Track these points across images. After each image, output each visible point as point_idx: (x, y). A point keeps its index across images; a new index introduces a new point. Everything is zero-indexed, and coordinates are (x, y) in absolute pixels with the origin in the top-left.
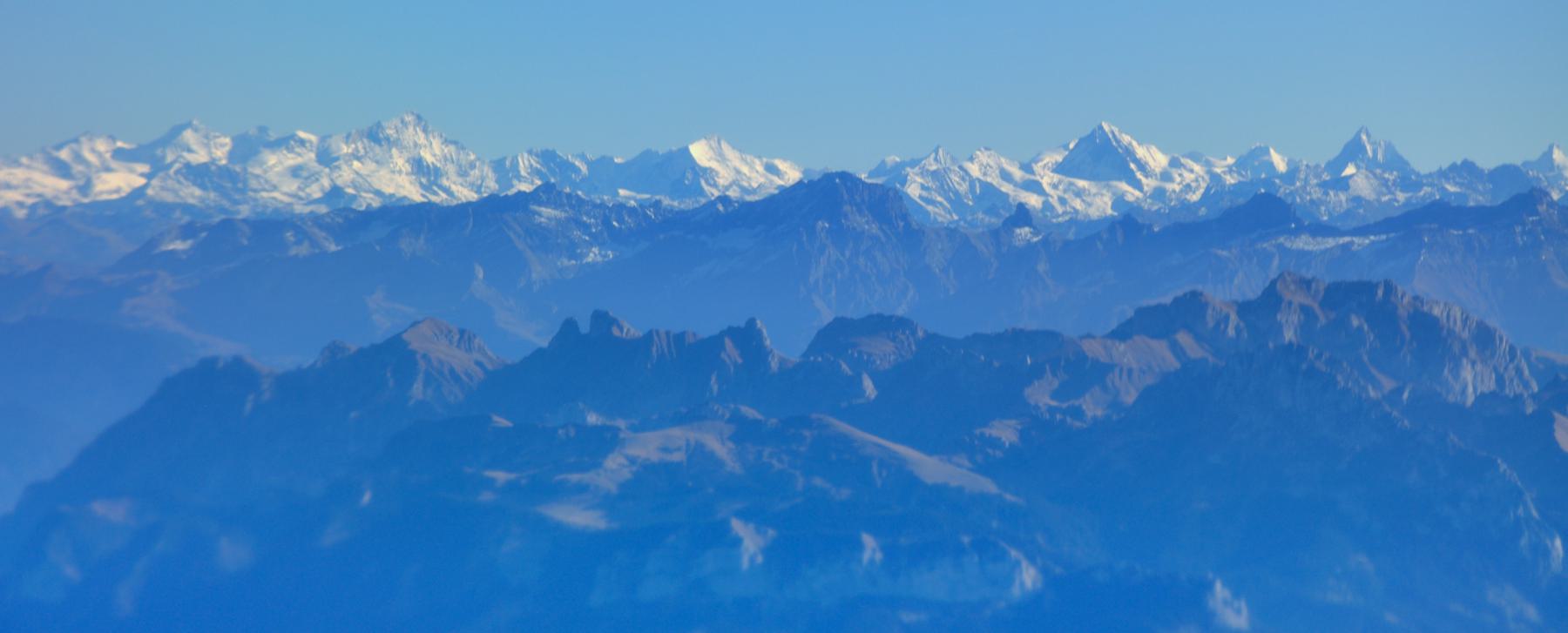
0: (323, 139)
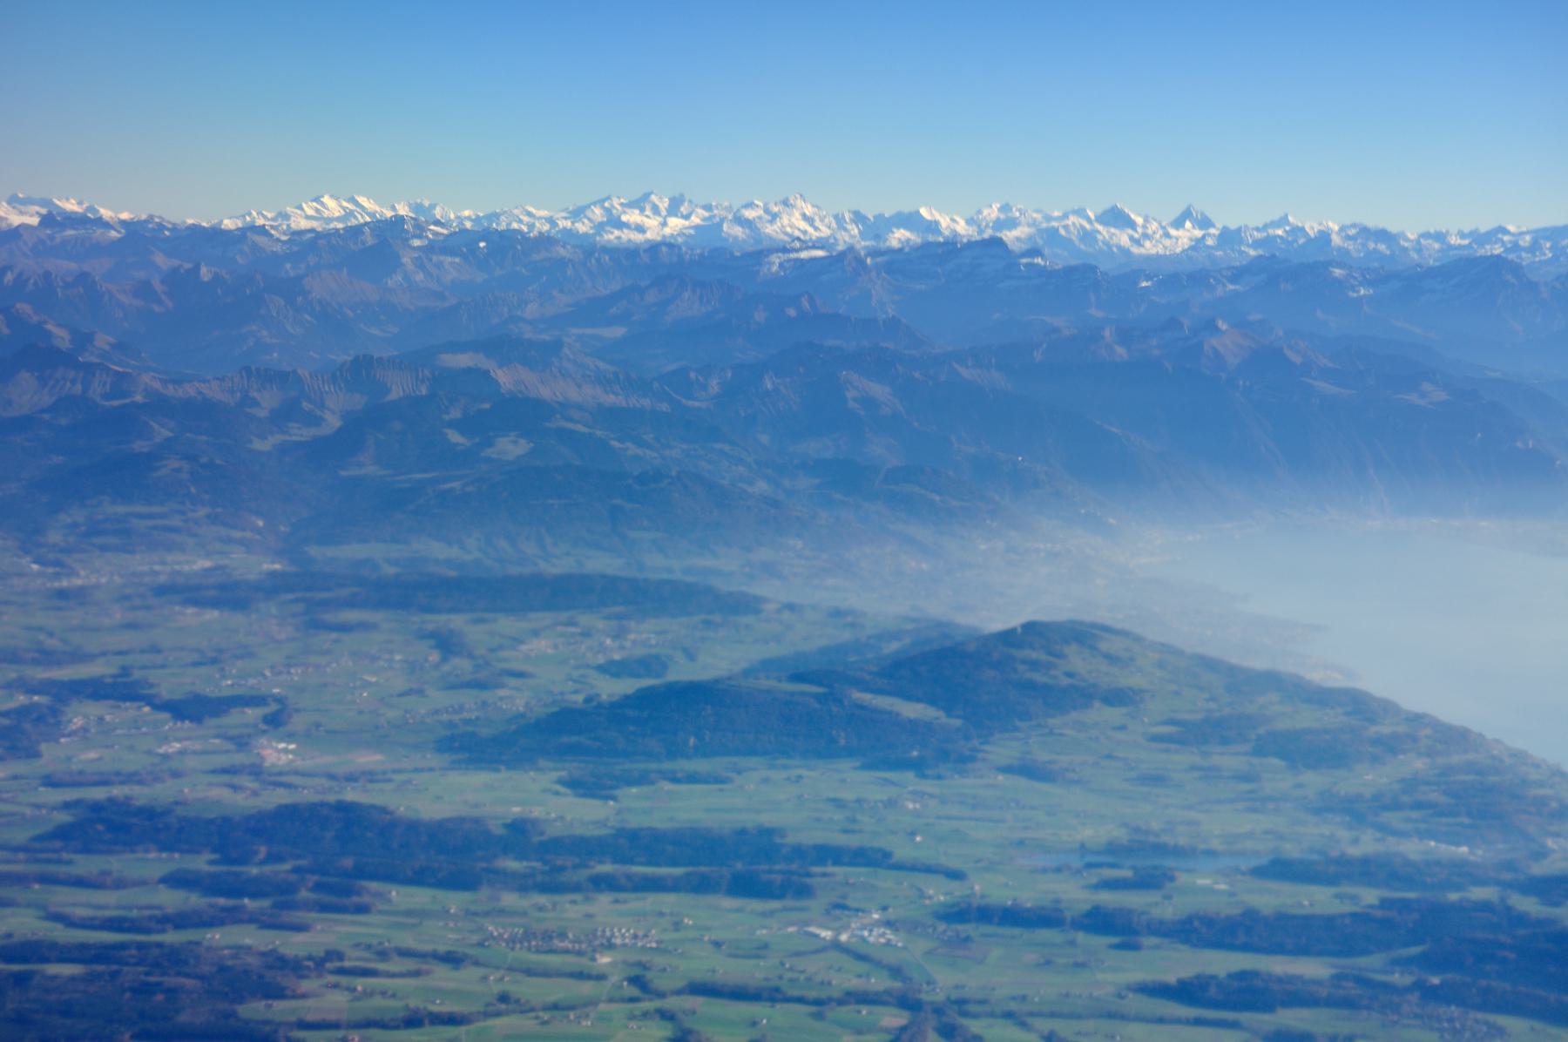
0: (765, 205)
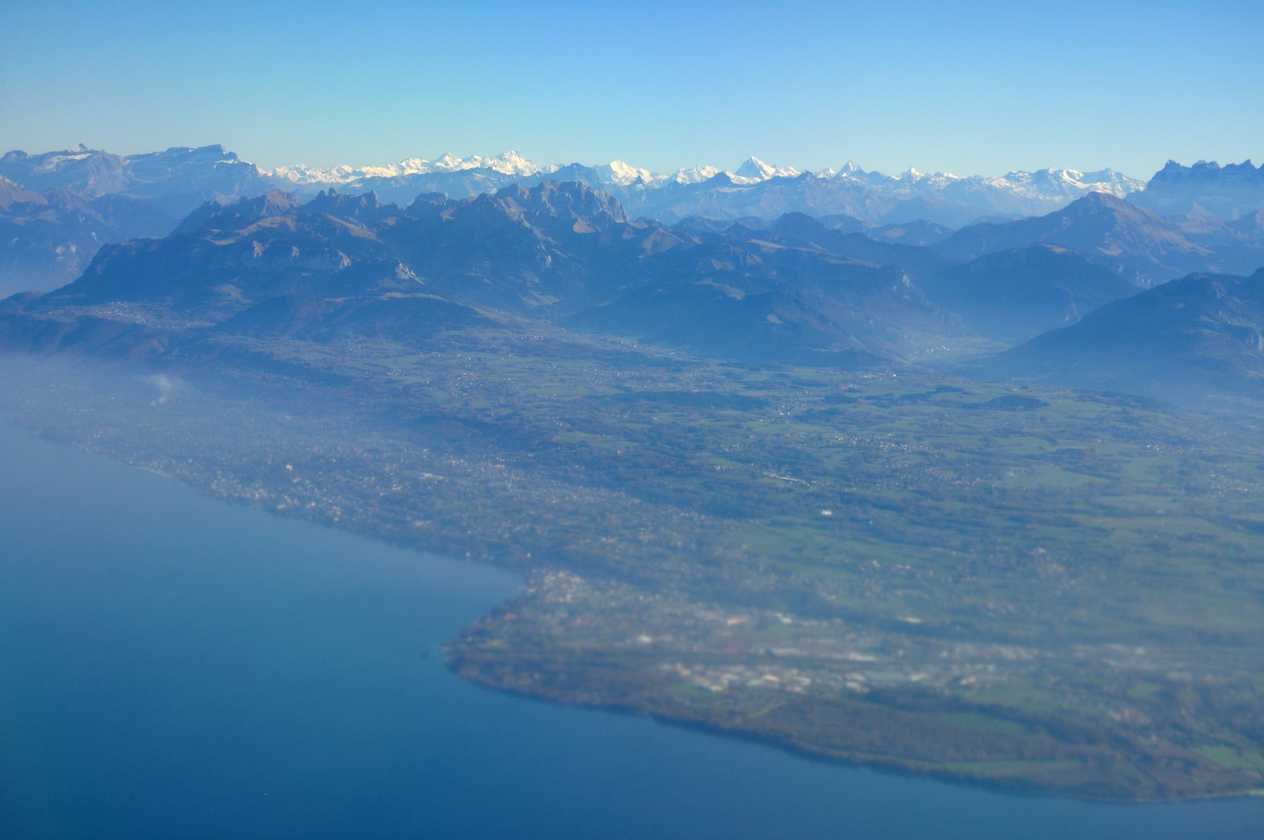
0: (483, 158)
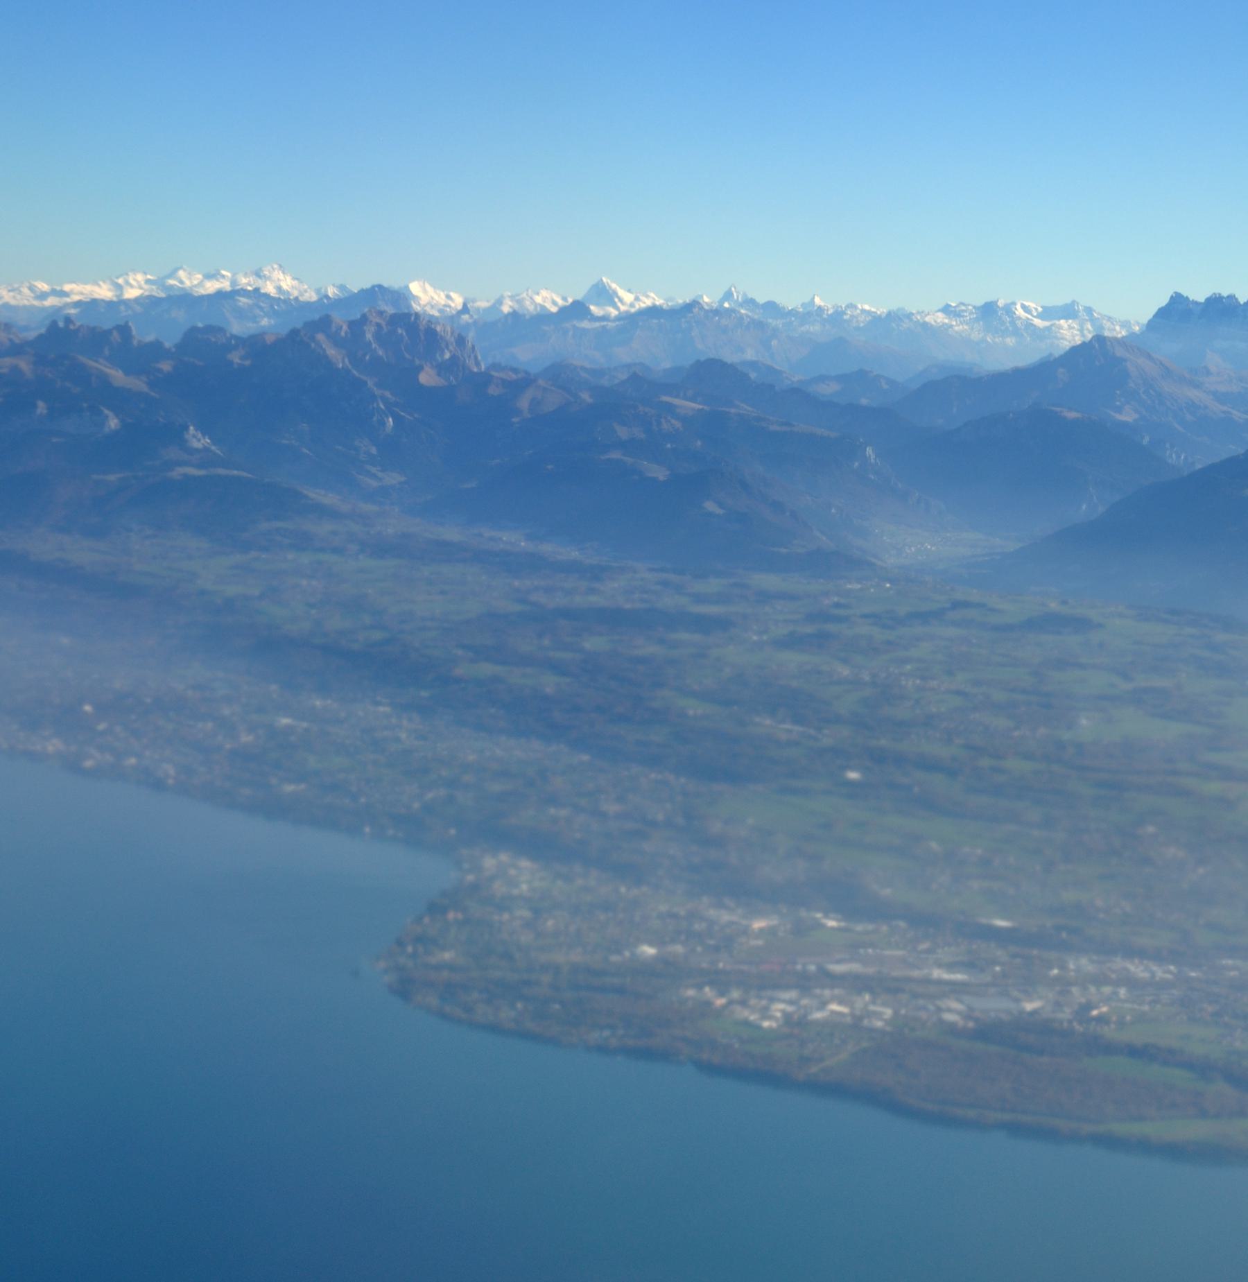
0: (234, 275)
